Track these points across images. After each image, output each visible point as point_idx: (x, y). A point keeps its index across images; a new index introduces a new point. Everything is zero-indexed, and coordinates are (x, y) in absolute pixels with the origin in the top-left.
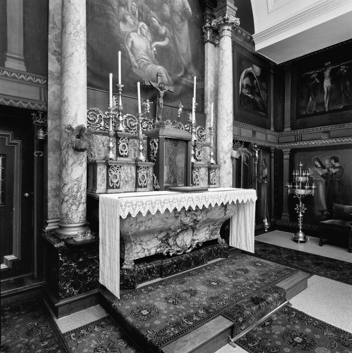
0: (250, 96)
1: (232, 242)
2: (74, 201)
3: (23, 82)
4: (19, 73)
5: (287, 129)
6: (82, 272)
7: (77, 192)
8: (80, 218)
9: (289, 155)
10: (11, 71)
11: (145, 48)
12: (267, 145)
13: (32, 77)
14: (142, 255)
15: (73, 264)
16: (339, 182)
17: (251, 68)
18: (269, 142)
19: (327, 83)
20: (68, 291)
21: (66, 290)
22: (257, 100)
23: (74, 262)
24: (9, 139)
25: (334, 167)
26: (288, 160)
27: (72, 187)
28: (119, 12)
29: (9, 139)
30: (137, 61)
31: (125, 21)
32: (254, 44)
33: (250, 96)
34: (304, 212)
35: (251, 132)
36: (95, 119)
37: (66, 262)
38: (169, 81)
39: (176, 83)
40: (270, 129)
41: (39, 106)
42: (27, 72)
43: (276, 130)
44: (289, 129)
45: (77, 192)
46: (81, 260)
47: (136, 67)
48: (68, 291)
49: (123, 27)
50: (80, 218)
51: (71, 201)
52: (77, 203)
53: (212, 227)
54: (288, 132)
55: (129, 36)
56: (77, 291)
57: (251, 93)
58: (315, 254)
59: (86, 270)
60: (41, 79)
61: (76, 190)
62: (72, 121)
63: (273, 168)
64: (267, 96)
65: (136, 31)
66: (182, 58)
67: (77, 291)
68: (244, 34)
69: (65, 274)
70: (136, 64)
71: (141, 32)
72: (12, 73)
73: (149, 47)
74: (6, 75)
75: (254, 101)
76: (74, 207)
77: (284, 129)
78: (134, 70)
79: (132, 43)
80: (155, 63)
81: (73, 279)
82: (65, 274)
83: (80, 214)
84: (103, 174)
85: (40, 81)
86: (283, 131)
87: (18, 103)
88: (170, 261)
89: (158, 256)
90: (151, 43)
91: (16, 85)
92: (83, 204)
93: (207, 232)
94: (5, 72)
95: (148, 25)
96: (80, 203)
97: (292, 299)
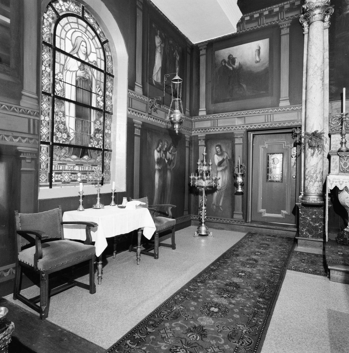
1: (262, 228)
2: (312, 179)
3: (289, 111)
6: (314, 225)
7: (313, 174)
8: (316, 190)
9: (241, 139)
10: (282, 108)
13: (293, 107)
15: (308, 218)
20: (304, 233)
21: (303, 232)
23: (309, 217)
24: (284, 145)
26: (241, 146)
27: (310, 171)
29: (284, 145)
36: (338, 123)
37: (303, 215)
41: (254, 127)
42: (291, 105)
44: (287, 103)
45: (313, 174)
46: (314, 217)
48: (304, 233)
50: (316, 190)
51: (309, 179)
52: (314, 181)
54: (203, 116)
56: (311, 236)
58: (205, 268)
59: (317, 225)
60: (298, 106)
61: (312, 172)
62: (311, 129)
67: (311, 236)
69: (303, 222)
72: (282, 108)
74: (280, 111)
76: (311, 183)
77: (279, 103)
81: (308, 227)
82: (303, 222)
83: (315, 188)
84: (336, 162)
85: (298, 108)
86: (198, 115)
87: (286, 124)
92: (318, 182)
94: (280, 109)
96: (315, 181)
97: (88, 284)
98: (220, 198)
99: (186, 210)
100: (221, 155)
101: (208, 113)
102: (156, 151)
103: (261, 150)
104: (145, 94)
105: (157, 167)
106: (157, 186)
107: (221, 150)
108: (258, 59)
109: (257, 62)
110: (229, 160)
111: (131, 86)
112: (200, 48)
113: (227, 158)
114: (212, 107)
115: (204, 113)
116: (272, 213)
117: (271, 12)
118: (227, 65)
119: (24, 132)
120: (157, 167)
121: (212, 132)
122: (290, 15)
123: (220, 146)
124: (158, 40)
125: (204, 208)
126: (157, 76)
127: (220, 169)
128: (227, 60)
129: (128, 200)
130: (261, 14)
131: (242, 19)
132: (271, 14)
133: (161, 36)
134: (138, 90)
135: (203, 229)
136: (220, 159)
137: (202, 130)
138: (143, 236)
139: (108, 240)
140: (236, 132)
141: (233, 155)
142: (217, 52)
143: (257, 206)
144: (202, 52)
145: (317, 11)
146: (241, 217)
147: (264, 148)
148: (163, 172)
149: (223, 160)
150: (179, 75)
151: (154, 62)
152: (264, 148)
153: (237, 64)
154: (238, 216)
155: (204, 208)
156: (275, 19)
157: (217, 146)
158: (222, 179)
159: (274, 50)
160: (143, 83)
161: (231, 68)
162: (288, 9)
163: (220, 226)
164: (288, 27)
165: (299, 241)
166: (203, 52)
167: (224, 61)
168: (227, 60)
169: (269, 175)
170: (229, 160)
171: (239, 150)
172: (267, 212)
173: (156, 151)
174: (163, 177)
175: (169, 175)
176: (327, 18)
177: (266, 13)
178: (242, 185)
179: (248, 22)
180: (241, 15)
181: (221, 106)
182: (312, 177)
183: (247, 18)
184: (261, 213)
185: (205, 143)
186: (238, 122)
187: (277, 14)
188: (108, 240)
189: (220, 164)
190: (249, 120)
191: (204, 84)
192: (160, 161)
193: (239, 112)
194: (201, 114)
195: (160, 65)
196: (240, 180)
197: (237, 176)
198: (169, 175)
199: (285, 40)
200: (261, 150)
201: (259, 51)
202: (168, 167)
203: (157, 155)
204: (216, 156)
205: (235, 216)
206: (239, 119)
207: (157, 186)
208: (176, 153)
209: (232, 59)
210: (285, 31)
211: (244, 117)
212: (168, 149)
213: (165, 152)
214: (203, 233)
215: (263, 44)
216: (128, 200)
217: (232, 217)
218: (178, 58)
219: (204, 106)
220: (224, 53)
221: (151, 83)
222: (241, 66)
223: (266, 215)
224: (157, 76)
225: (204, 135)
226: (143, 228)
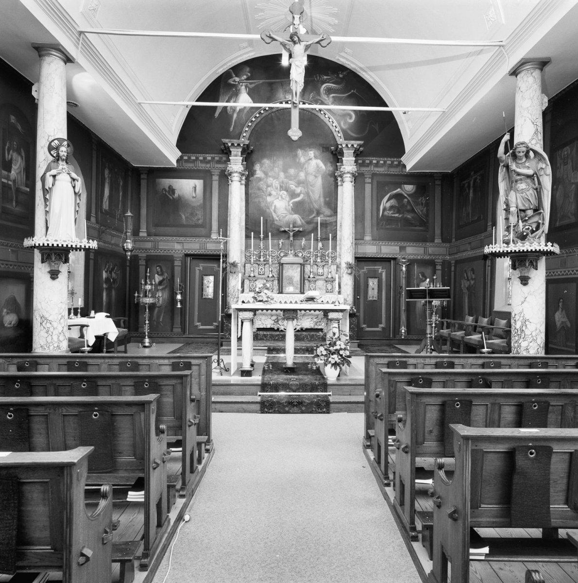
0: (397, 215)
4: (440, 244)
5: (454, 240)
11: (284, 206)
12: (427, 257)
14: (262, 327)
16: (474, 293)
17: (399, 190)
18: (430, 255)
19: (471, 195)
22: (409, 216)
25: (472, 279)
28: (266, 191)
30: (278, 217)
31: (270, 195)
32: (404, 166)
33: (397, 215)
34: (437, 322)
35: (397, 248)
38: (302, 223)
39: (309, 223)
40: (433, 241)
43: (444, 240)
47: (277, 220)
49: (269, 199)
53: (315, 320)
55: (273, 203)
57: (399, 212)
63: (92, 269)
64: (427, 210)
65: (278, 198)
66: (314, 204)
68: (374, 162)
70: (277, 219)
71: (282, 197)
73: (287, 205)
75: (406, 220)
76: (232, 299)
78: (276, 222)
79: (275, 206)
80: (291, 214)
88: (278, 333)
89: (272, 329)
90: (289, 202)
91: (214, 245)
93: (312, 322)
95: (287, 191)
98: (160, 315)
99: (438, 185)
100: (162, 274)
101: (149, 235)
102: (104, 272)
103: (197, 272)
104: (97, 222)
105: (105, 286)
106: (104, 304)
107: (161, 270)
108: (194, 195)
109: (194, 197)
110: (169, 280)
111: (88, 218)
112: (141, 172)
113: (167, 277)
114: (153, 230)
115: (145, 235)
116: (157, 168)
117: (205, 158)
118: (167, 194)
119: (522, 360)
120: (105, 286)
121: (153, 252)
122: (219, 166)
123: (160, 267)
124: (107, 172)
125: (147, 322)
126: (106, 205)
127: (160, 287)
128: (167, 189)
129: (95, 313)
130: (197, 158)
131: (181, 157)
132: (204, 161)
133: (109, 169)
134: (93, 219)
135: (147, 340)
136: (161, 278)
137: (143, 250)
138: (108, 339)
139: (97, 337)
140: (175, 255)
141: (173, 276)
142: (157, 180)
143: (193, 320)
144: (142, 176)
145: (236, 175)
146: (180, 330)
147: (200, 270)
148: (109, 290)
149: (163, 280)
150: (131, 212)
151: (104, 193)
152: (200, 270)
153: (176, 195)
154: (177, 330)
155: (147, 322)
156: (208, 165)
157: (157, 267)
158: (162, 296)
159: (207, 188)
160: (96, 213)
161: (171, 197)
162: (217, 161)
163: (160, 340)
164: (217, 175)
165: (224, 343)
166: (143, 176)
167: (164, 189)
168: (167, 189)
169: (204, 293)
170: (169, 280)
171: (178, 270)
172: (368, 327)
173: (104, 272)
174: (109, 296)
175: (113, 293)
176: (244, 178)
177: (201, 158)
178: (181, 301)
179: (186, 161)
180: (180, 154)
181: (162, 230)
182: (232, 295)
183: (186, 158)
184: (197, 326)
185: (146, 263)
186: (177, 247)
187: (209, 162)
188: (97, 337)
189: (160, 283)
190: (187, 246)
191: (145, 206)
192: (107, 279)
193: (178, 238)
194: (141, 234)
195: (108, 194)
196: (179, 297)
197: (176, 294)
198: (113, 293)
199: (215, 185)
200: (197, 272)
201: (195, 188)
202: (113, 286)
203: (105, 275)
204: (156, 275)
205: (175, 330)
206: (178, 244)
207: (104, 304)
208: (119, 272)
209: (172, 190)
210: (216, 178)
211: (183, 243)
212: (113, 269)
213: (111, 272)
214: (147, 344)
215: (199, 183)
216: (95, 313)
217: (172, 331)
218: (121, 184)
219: (145, 228)
220: (166, 182)
221: (101, 210)
222: (180, 198)
223: (201, 327)
224: (106, 205)
225: (144, 255)
226: (108, 333)
